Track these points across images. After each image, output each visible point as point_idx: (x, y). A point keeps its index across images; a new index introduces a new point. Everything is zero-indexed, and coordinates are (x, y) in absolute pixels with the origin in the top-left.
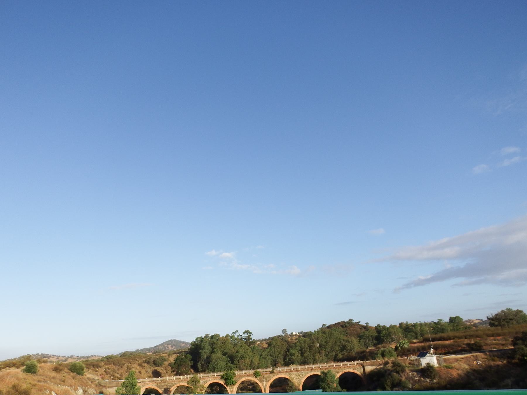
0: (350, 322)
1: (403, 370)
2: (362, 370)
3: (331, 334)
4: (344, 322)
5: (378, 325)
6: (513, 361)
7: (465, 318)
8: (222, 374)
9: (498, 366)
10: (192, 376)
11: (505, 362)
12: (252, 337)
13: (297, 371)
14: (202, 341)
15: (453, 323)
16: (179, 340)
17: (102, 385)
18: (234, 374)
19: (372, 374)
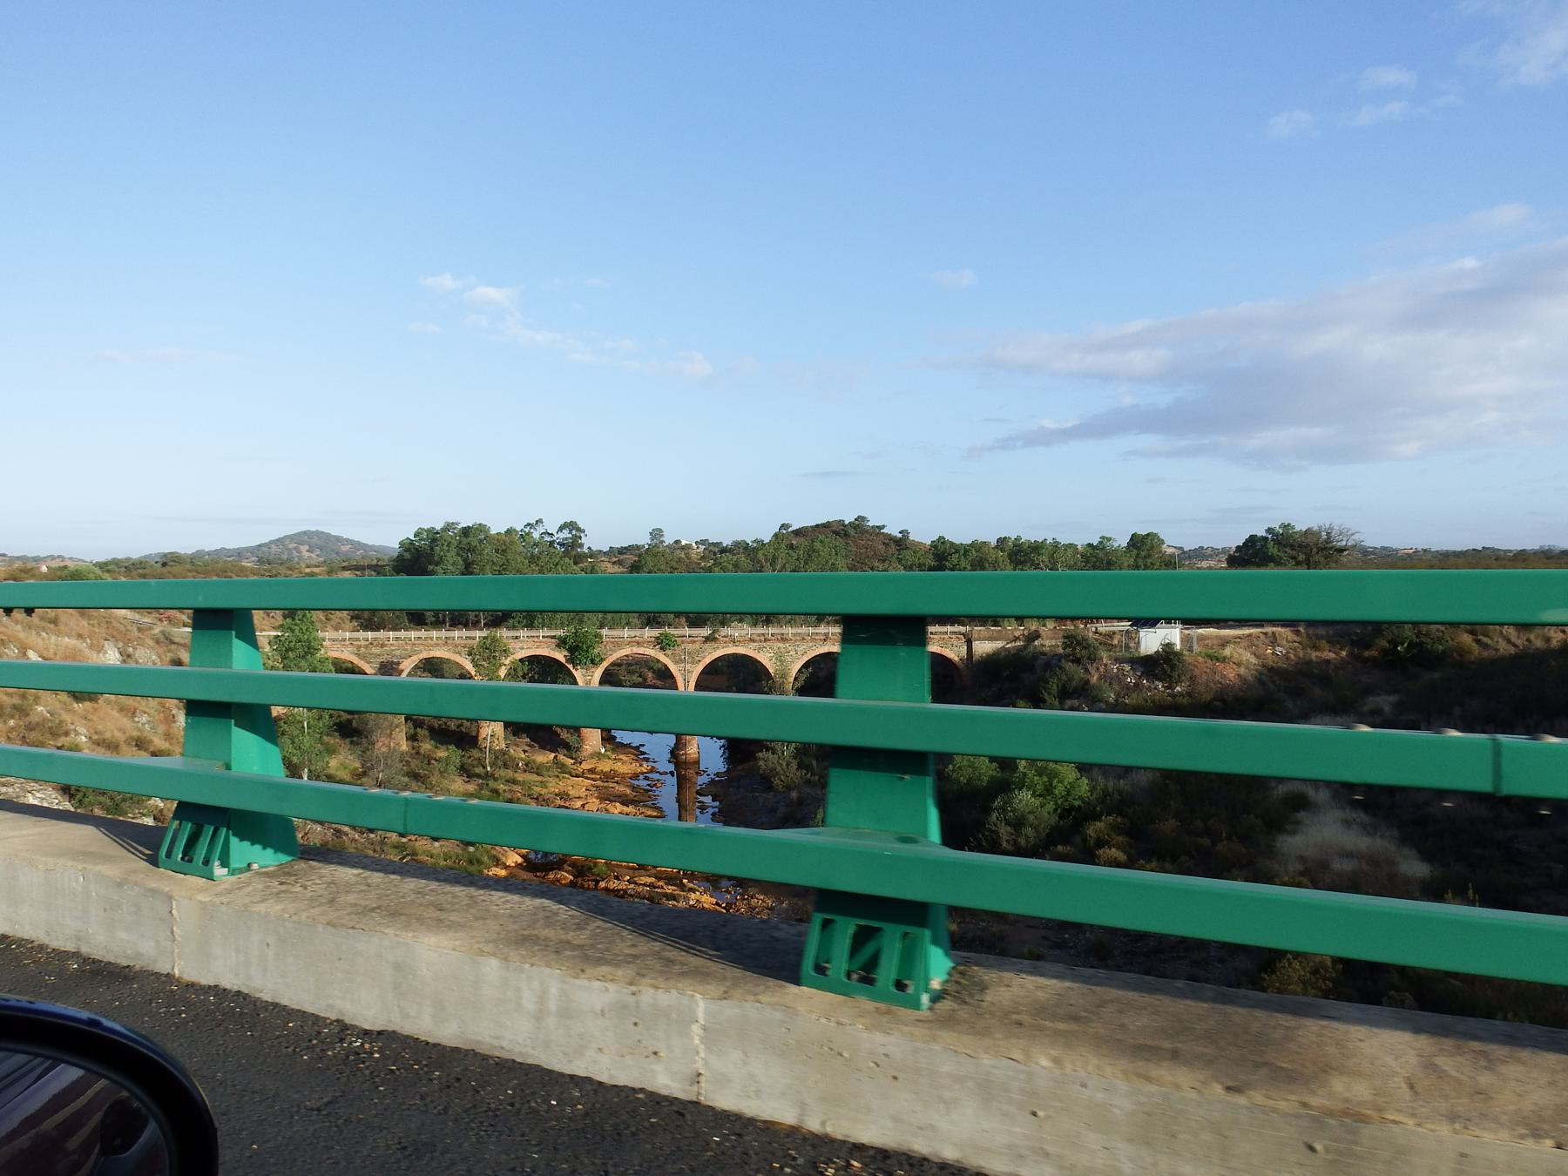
0: (859, 524)
1: (1093, 659)
3: (812, 550)
4: (841, 522)
5: (941, 538)
6: (1366, 654)
8: (560, 633)
9: (1328, 662)
11: (1344, 653)
12: (583, 540)
13: (784, 639)
14: (434, 540)
16: (335, 532)
18: (598, 636)
19: (992, 664)
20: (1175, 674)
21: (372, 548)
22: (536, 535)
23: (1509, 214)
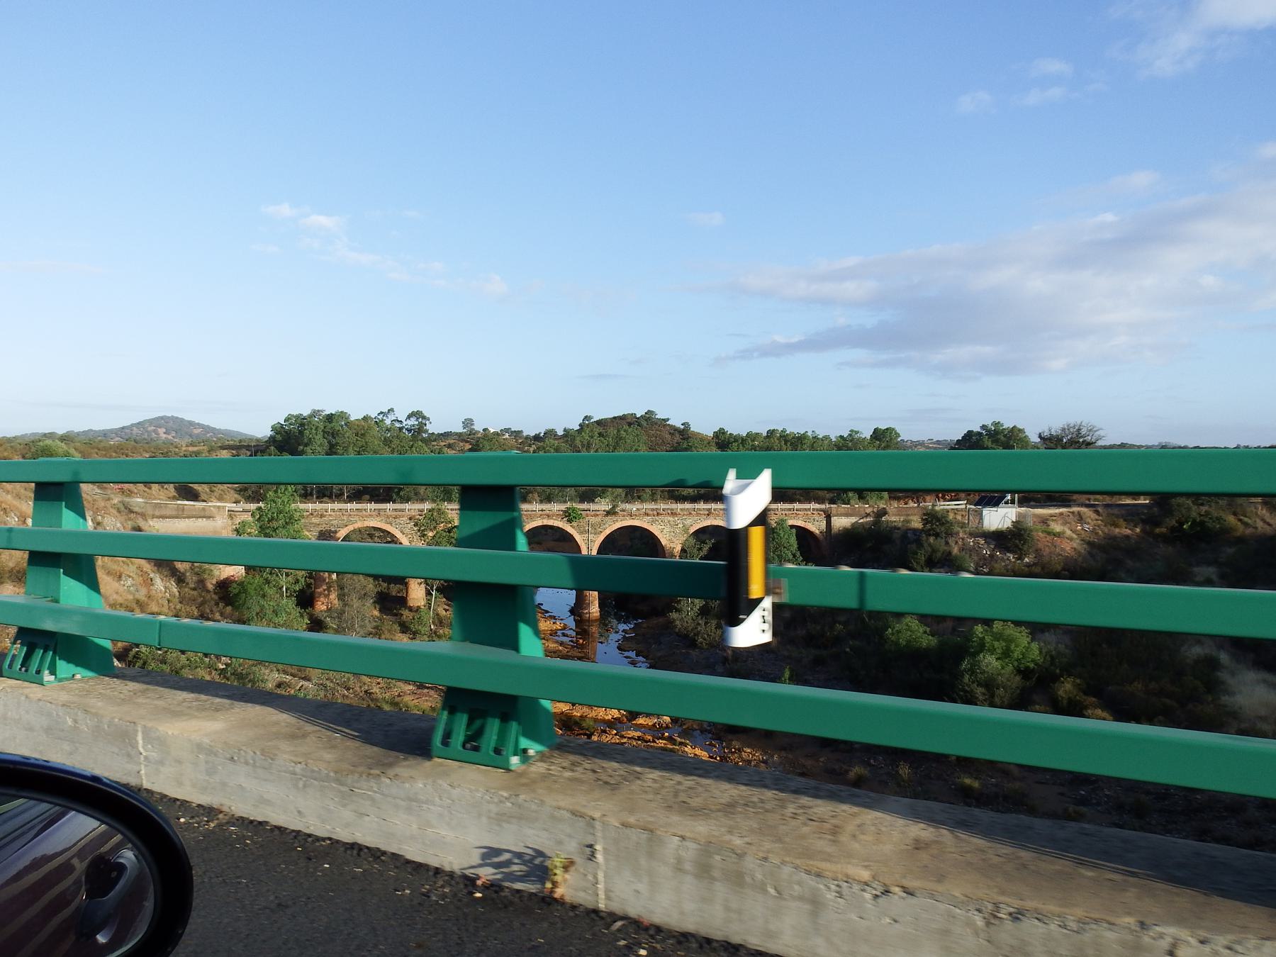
1: (950, 534)
2: (823, 525)
4: (633, 415)
5: (721, 429)
6: (1157, 530)
7: (1110, 435)
9: (1127, 537)
10: (427, 506)
11: (1138, 530)
12: (428, 427)
13: (673, 514)
14: (302, 425)
15: (879, 440)
16: (188, 417)
17: (136, 509)
20: (1025, 548)
21: (219, 431)
22: (388, 422)
23: (1141, 179)
